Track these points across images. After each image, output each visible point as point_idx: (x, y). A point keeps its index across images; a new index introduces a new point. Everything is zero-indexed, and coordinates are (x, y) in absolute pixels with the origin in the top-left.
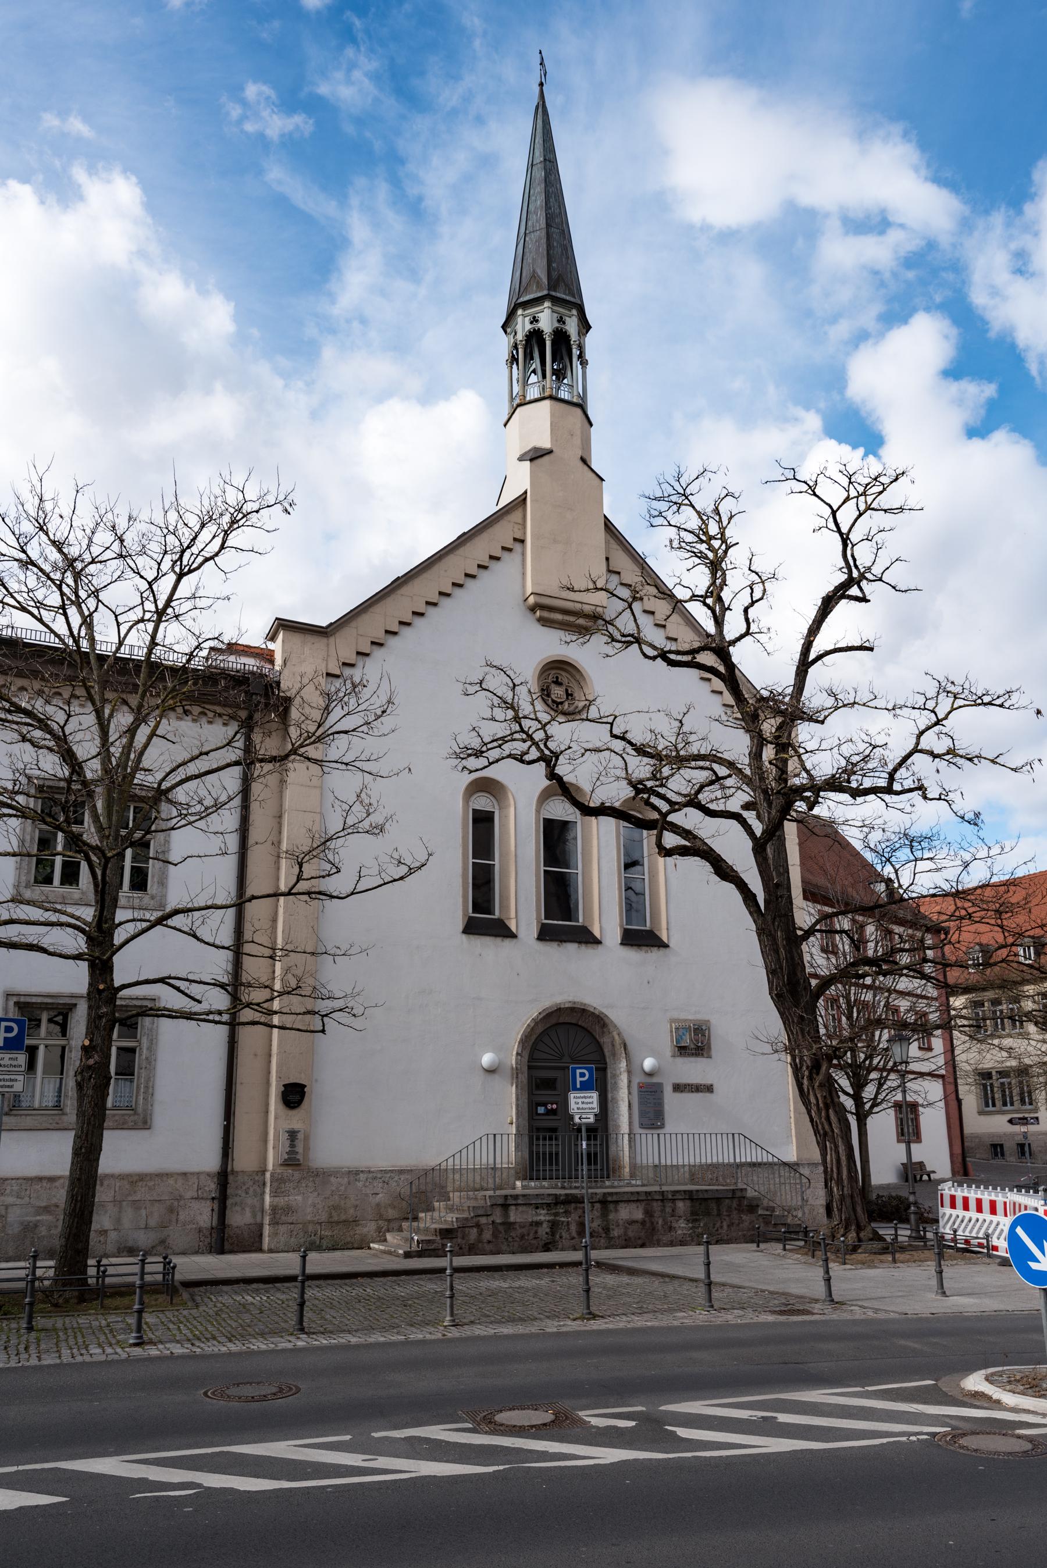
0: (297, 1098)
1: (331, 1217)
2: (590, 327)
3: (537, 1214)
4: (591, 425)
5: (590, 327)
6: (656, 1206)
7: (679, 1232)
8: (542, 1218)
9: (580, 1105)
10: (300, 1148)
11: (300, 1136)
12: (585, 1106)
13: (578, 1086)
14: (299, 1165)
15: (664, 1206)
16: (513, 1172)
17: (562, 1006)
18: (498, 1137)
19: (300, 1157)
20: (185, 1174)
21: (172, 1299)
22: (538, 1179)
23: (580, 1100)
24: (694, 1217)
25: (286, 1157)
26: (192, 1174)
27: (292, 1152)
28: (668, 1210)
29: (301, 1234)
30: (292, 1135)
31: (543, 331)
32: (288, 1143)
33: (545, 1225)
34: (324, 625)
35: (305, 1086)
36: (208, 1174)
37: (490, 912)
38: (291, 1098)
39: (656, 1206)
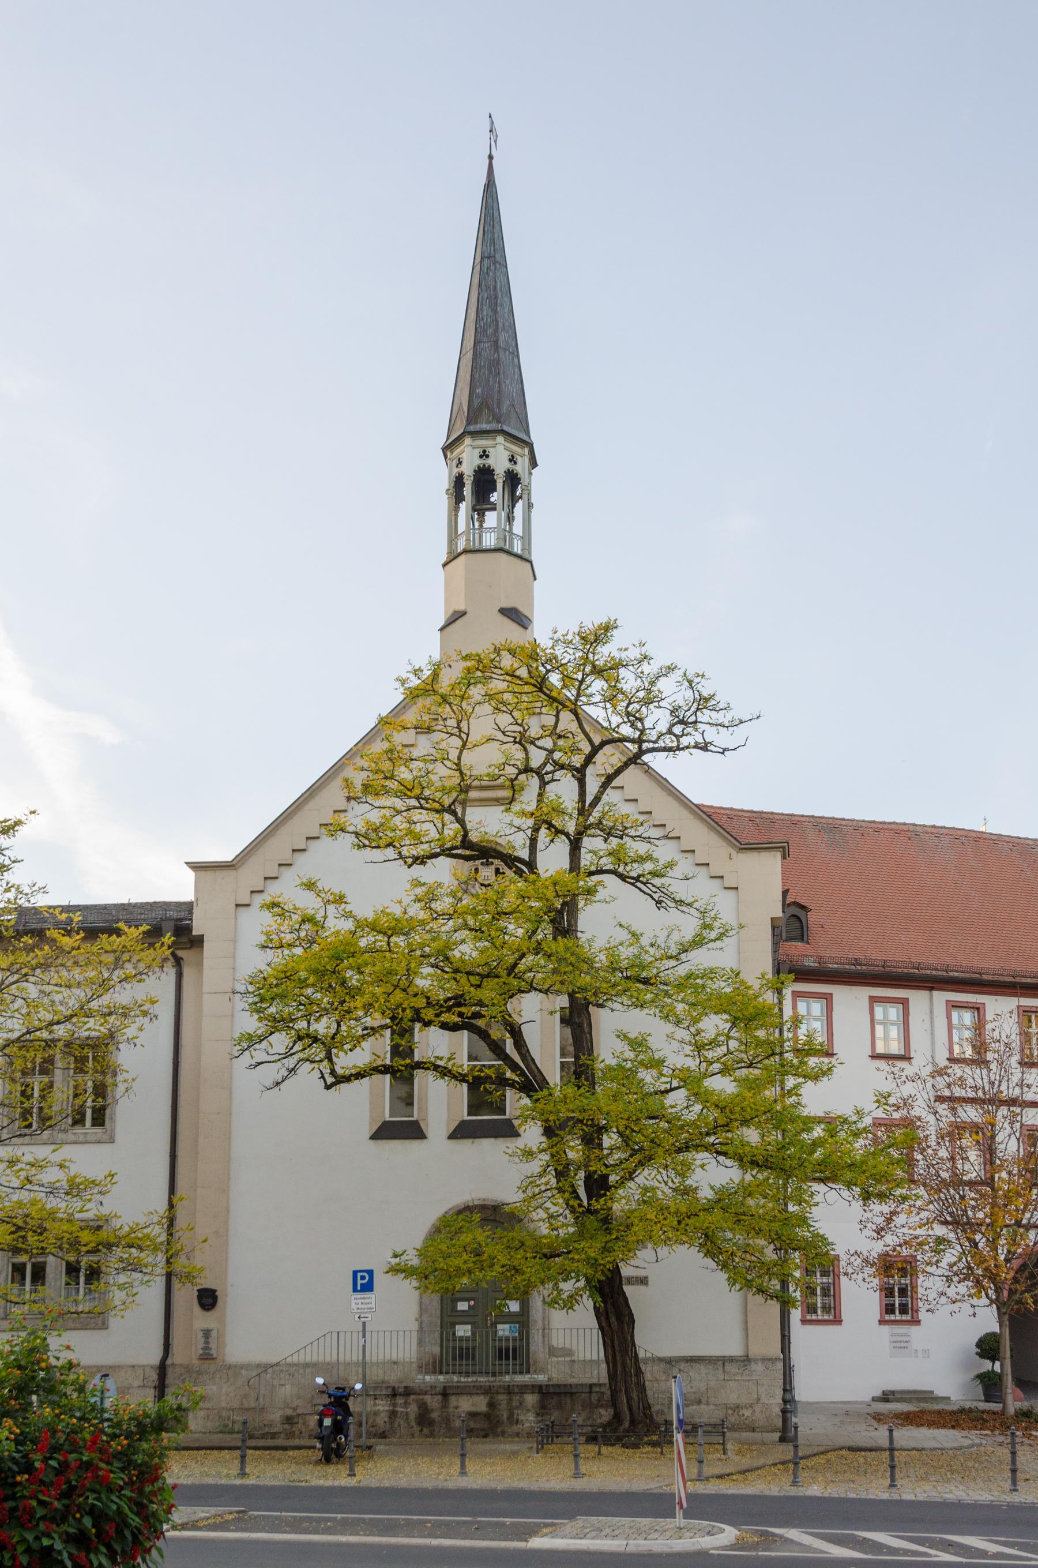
0: (210, 1301)
1: (242, 1404)
2: (537, 465)
3: (375, 1405)
4: (535, 579)
5: (537, 465)
6: (502, 1398)
7: (527, 1425)
8: (381, 1408)
9: (360, 1306)
10: (213, 1345)
11: (214, 1334)
12: (364, 1306)
13: (359, 1288)
14: (214, 1359)
15: (510, 1399)
16: (415, 1366)
17: (471, 1204)
18: (342, 1335)
19: (214, 1352)
20: (133, 1366)
21: (463, 1466)
22: (447, 1373)
23: (360, 1301)
24: (542, 1409)
25: (201, 1352)
26: (139, 1366)
27: (206, 1348)
28: (515, 1403)
29: (217, 1418)
30: (207, 1333)
31: (520, 479)
32: (203, 1340)
33: (383, 1415)
34: (230, 859)
35: (215, 1291)
36: (152, 1367)
37: (503, 1111)
38: (205, 1301)
39: (502, 1398)
